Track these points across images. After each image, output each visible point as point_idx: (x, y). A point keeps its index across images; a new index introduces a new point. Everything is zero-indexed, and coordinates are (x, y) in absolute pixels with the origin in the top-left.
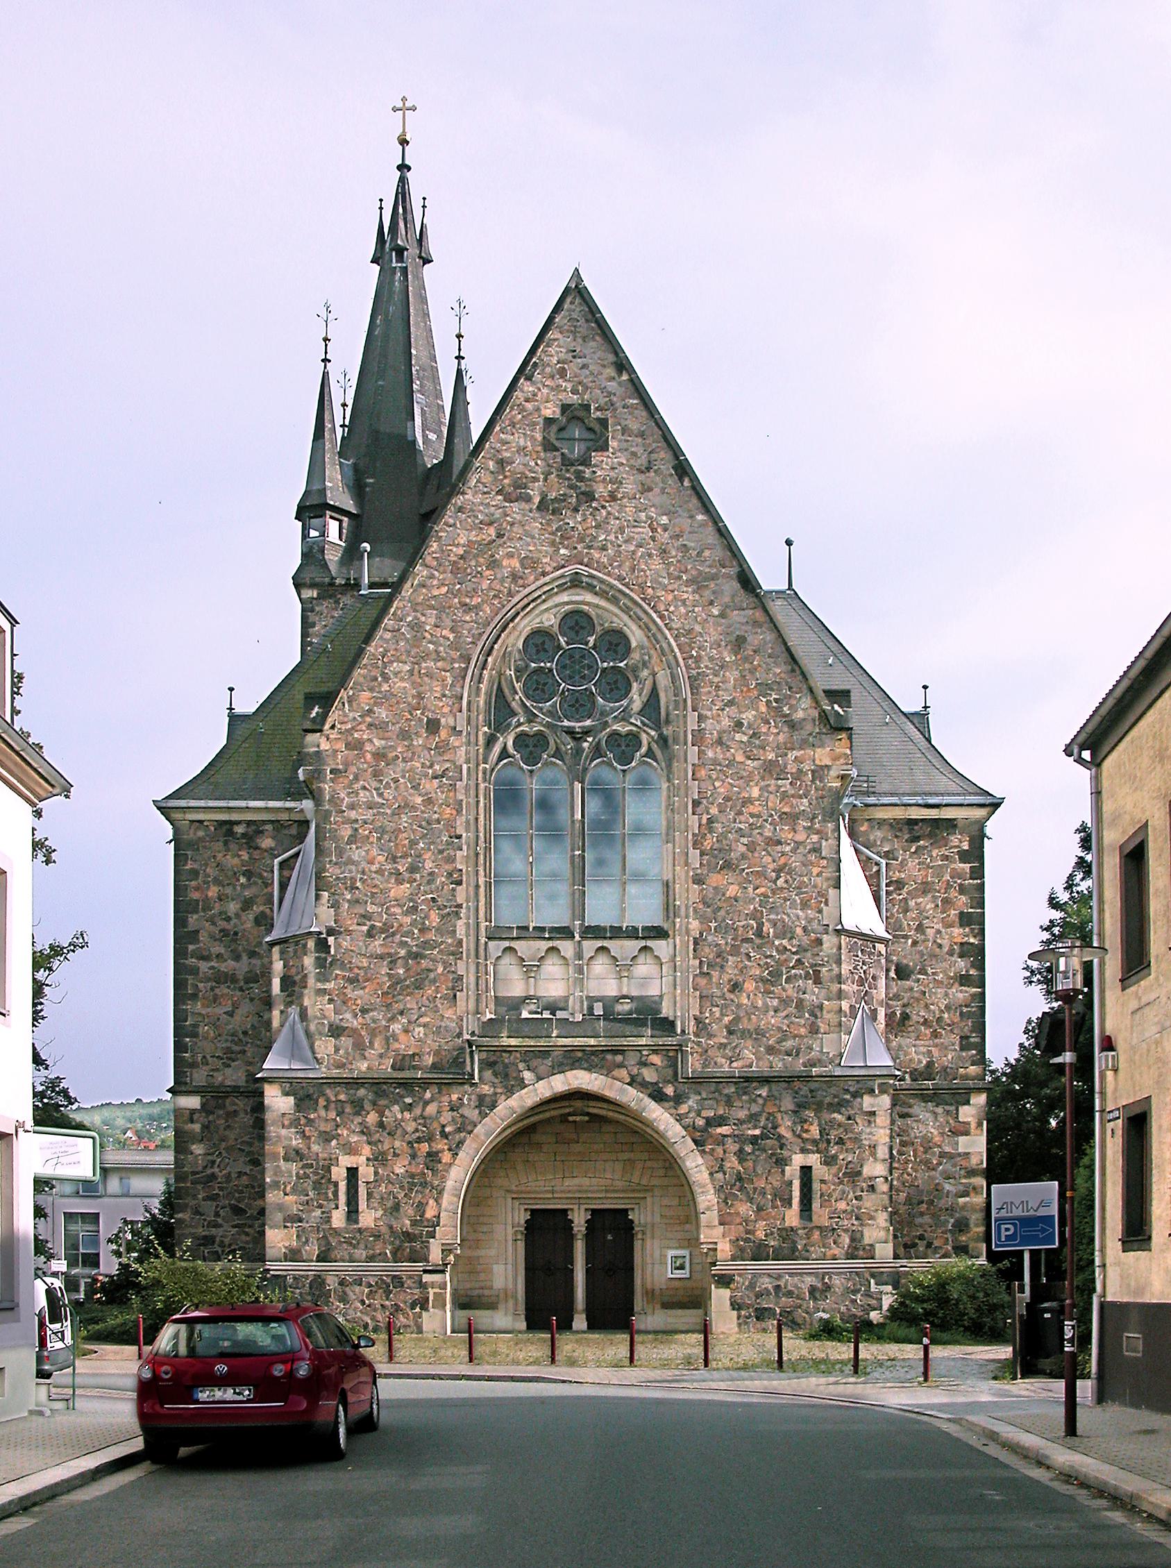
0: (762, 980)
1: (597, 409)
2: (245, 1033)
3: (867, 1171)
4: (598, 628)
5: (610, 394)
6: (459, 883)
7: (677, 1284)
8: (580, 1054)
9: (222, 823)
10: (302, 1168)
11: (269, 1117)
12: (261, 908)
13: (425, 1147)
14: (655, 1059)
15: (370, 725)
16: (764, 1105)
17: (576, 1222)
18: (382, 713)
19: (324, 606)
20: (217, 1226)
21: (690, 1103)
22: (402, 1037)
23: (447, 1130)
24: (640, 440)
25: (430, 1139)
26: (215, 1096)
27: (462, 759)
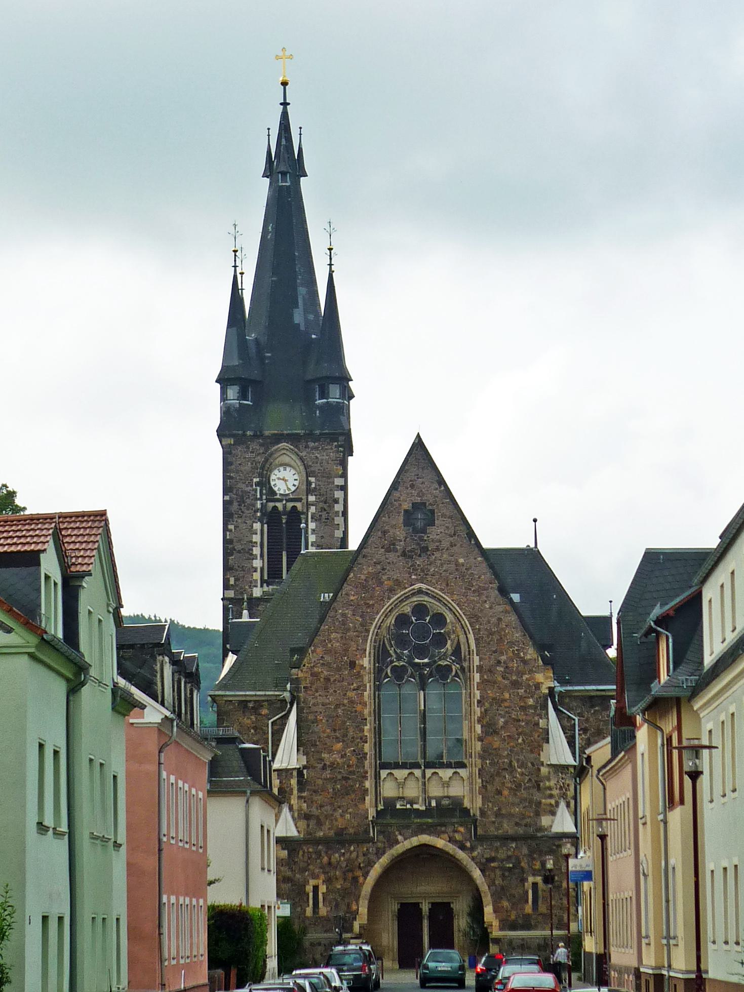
4: (431, 613)
5: (436, 497)
9: (241, 702)
13: (350, 875)
15: (323, 664)
18: (328, 658)
19: (239, 450)
22: (340, 820)
25: (352, 871)
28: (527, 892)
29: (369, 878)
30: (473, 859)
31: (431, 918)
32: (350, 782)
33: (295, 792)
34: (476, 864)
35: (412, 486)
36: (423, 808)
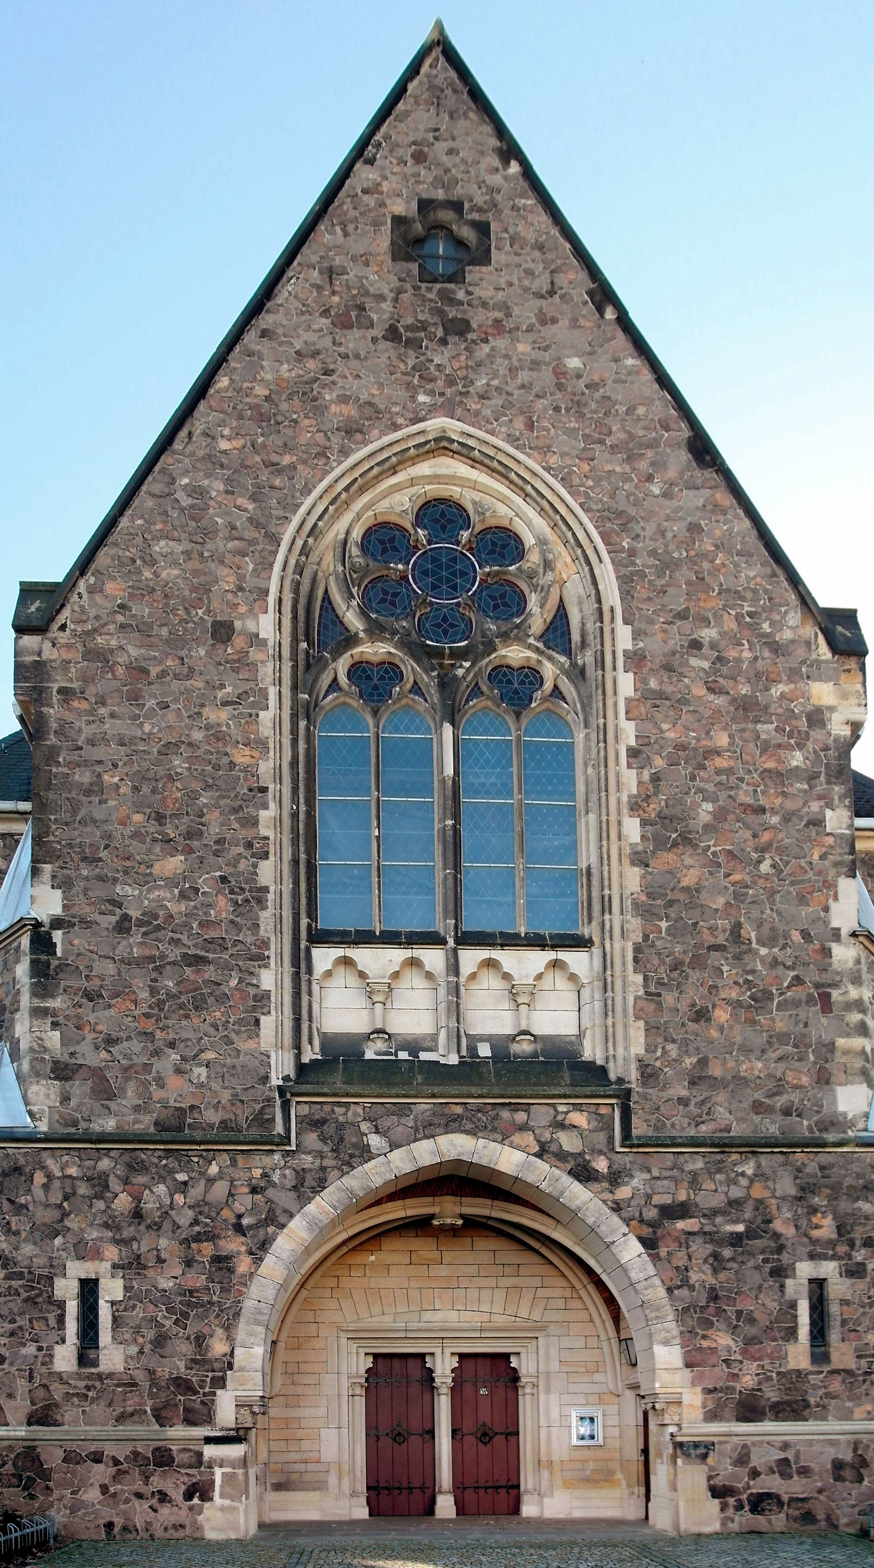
0: (738, 1004)
1: (472, 210)
5: (492, 190)
6: (265, 856)
7: (587, 1454)
13: (207, 1249)
15: (122, 626)
16: (749, 1188)
18: (141, 610)
21: (635, 1182)
23: (245, 1221)
27: (269, 679)
28: (793, 1305)
29: (269, 1260)
30: (617, 1208)
31: (456, 1390)
32: (210, 972)
33: (25, 1000)
34: (627, 1222)
35: (419, 157)
36: (453, 1059)
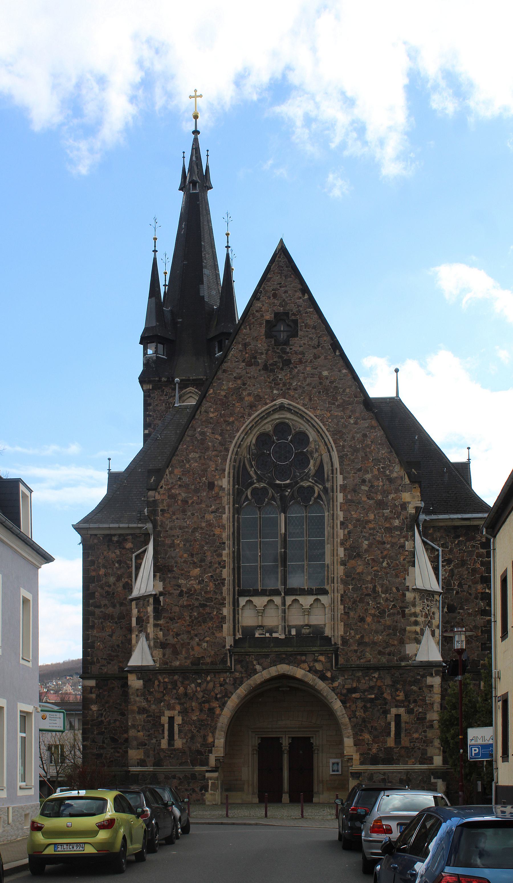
2: (118, 646)
3: (429, 717)
4: (293, 432)
5: (299, 306)
6: (224, 567)
8: (284, 656)
10: (147, 717)
11: (130, 691)
12: (126, 580)
13: (207, 705)
14: (322, 658)
15: (180, 486)
16: (376, 682)
17: (284, 744)
18: (186, 479)
20: (103, 748)
21: (339, 681)
22: (196, 648)
24: (314, 330)
26: (103, 680)
27: (226, 503)
